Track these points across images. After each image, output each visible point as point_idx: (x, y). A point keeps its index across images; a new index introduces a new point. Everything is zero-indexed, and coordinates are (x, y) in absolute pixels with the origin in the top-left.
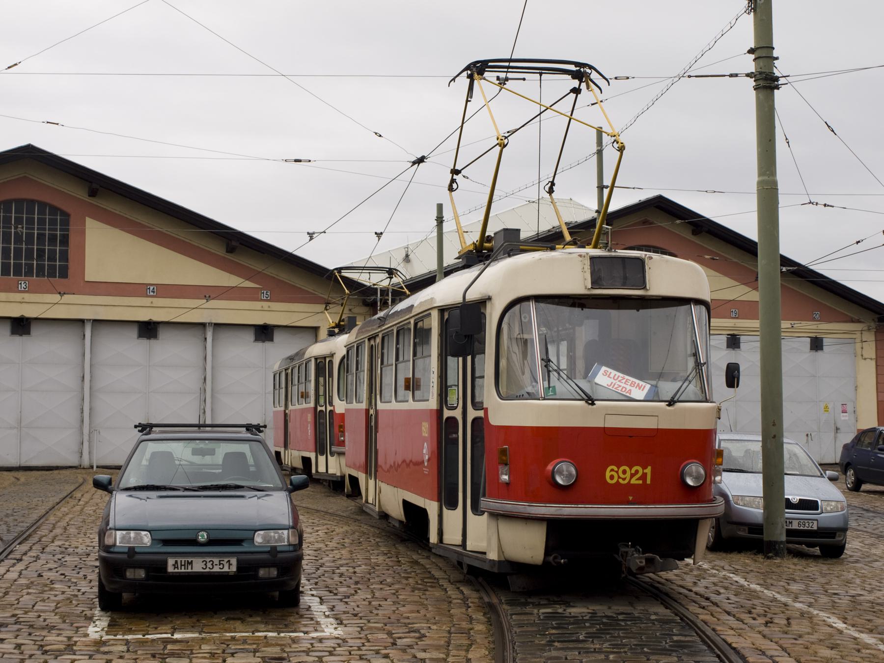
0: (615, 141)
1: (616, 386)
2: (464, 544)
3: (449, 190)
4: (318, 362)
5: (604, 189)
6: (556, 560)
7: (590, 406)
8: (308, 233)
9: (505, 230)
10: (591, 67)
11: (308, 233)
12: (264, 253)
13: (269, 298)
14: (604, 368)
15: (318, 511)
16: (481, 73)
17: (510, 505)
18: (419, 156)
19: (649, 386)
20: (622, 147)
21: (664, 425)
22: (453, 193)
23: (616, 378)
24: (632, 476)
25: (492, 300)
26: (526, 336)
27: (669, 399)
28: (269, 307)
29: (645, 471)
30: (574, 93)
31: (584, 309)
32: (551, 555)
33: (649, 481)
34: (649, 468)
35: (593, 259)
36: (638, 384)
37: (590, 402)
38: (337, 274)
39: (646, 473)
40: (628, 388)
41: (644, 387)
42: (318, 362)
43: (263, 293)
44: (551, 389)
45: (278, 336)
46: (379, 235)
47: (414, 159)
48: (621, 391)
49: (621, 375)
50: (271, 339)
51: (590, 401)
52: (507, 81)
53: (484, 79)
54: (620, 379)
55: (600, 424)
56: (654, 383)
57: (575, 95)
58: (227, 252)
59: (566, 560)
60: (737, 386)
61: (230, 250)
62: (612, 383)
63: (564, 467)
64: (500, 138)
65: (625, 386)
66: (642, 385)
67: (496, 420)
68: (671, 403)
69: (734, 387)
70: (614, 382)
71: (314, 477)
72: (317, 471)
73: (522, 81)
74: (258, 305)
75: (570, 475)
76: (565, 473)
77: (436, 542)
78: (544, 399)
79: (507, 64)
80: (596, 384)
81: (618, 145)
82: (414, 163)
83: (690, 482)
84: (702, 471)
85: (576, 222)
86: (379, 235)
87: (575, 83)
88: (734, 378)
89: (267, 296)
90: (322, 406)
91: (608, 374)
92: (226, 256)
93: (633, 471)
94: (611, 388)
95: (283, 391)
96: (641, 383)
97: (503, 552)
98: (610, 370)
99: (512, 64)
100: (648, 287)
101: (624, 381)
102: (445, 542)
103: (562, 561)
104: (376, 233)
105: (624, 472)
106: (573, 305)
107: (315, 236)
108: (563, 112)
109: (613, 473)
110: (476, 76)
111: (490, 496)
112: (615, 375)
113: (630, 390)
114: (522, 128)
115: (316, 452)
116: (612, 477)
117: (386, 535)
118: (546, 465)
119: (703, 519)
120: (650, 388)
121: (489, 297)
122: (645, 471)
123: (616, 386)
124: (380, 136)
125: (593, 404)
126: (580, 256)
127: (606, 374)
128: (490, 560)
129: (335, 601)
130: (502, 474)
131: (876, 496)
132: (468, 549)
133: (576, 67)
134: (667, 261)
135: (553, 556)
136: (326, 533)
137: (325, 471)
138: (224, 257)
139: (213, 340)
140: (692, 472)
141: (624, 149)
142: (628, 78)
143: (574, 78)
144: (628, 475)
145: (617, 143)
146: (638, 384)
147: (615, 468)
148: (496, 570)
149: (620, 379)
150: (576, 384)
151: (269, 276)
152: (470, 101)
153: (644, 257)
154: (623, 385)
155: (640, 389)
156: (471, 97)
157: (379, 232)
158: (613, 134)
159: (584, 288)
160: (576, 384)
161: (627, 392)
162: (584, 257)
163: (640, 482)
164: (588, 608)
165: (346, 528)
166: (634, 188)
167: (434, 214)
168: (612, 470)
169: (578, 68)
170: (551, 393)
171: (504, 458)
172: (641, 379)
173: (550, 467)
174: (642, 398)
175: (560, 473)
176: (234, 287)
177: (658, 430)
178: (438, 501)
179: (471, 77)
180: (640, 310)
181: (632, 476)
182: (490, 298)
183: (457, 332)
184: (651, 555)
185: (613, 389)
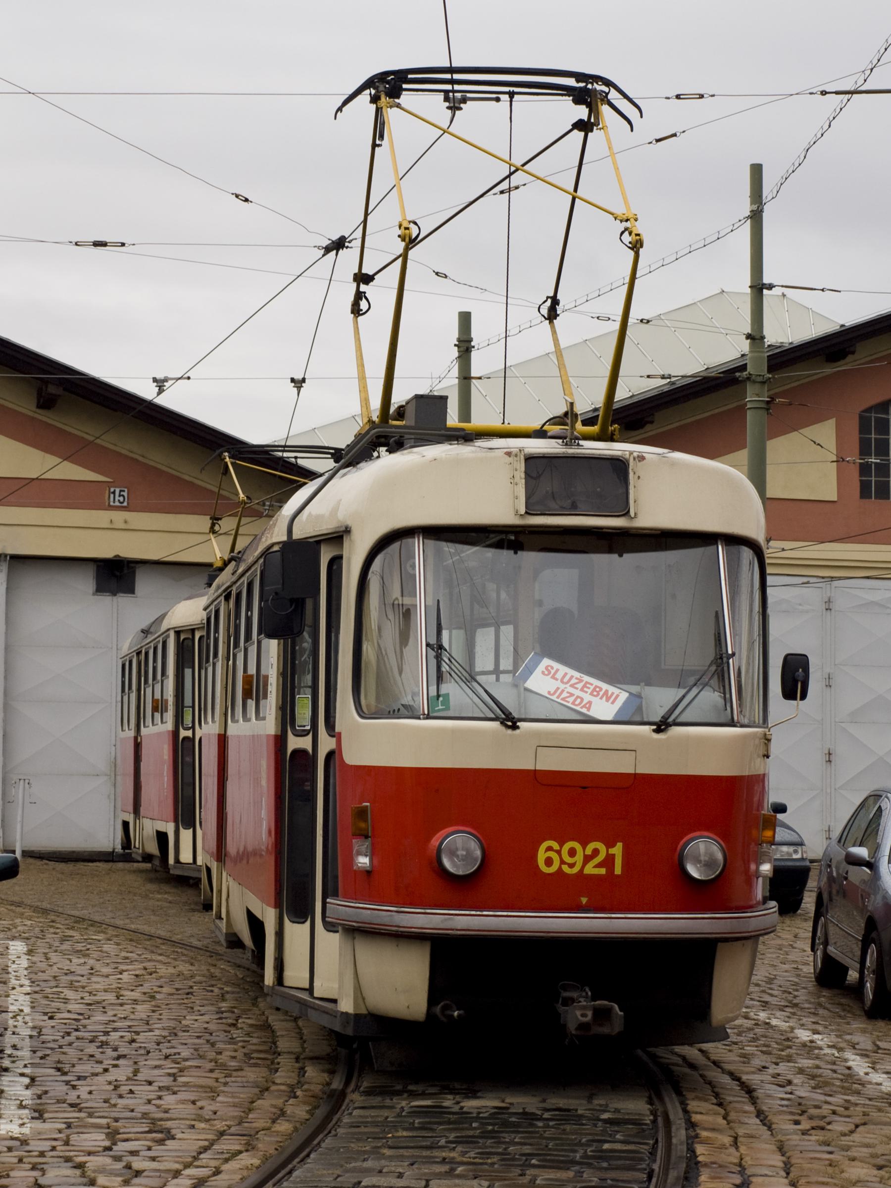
0: (626, 229)
1: (565, 695)
2: (310, 990)
3: (352, 312)
4: (182, 638)
5: (765, 292)
6: (449, 1012)
7: (510, 731)
8: (155, 380)
9: (418, 397)
10: (608, 83)
11: (155, 380)
12: (115, 410)
13: (125, 504)
14: (546, 662)
15: (151, 937)
16: (395, 93)
17: (369, 912)
18: (335, 237)
19: (626, 695)
20: (637, 241)
21: (645, 768)
22: (360, 318)
23: (566, 680)
24: (587, 859)
25: (352, 534)
26: (407, 601)
27: (657, 719)
28: (126, 522)
29: (612, 851)
30: (580, 130)
31: (519, 553)
32: (438, 1004)
33: (618, 870)
34: (620, 845)
35: (531, 460)
36: (607, 691)
37: (510, 723)
38: (227, 460)
39: (614, 855)
40: (587, 697)
41: (618, 696)
42: (182, 638)
43: (114, 493)
44: (441, 699)
45: (144, 583)
46: (298, 383)
47: (326, 243)
48: (573, 703)
49: (577, 674)
50: (131, 590)
51: (510, 721)
52: (465, 103)
53: (398, 106)
54: (574, 681)
55: (526, 764)
56: (635, 689)
57: (583, 134)
58: (39, 406)
59: (461, 1012)
60: (803, 697)
61: (46, 403)
62: (558, 688)
63: (459, 843)
64: (405, 224)
65: (581, 694)
66: (613, 693)
67: (354, 756)
68: (662, 726)
69: (795, 698)
70: (562, 686)
71: (172, 872)
72: (177, 860)
73: (494, 103)
74: (101, 517)
75: (469, 853)
76: (461, 853)
77: (271, 985)
78: (428, 717)
79: (448, 76)
80: (526, 689)
81: (630, 239)
82: (328, 250)
83: (694, 871)
84: (719, 856)
85: (791, 343)
86: (298, 383)
87: (582, 112)
88: (795, 682)
89: (121, 499)
90: (306, 733)
91: (553, 672)
92: (36, 416)
93: (589, 851)
94: (554, 698)
95: (133, 696)
96: (611, 689)
97: (364, 999)
98: (556, 665)
99: (456, 76)
100: (632, 514)
101: (580, 686)
102: (288, 982)
103: (456, 1014)
104: (293, 380)
105: (572, 853)
106: (499, 545)
107: (167, 384)
108: (541, 175)
109: (551, 854)
110: (384, 100)
111: (348, 896)
112: (566, 674)
113: (590, 703)
114: (481, 199)
115: (176, 821)
116: (549, 862)
117: (253, 982)
118: (429, 839)
119: (726, 940)
120: (628, 698)
121: (346, 528)
122: (612, 851)
123: (565, 695)
124: (246, 200)
125: (514, 727)
126: (509, 454)
127: (550, 672)
128: (342, 1013)
129: (57, 1083)
130: (359, 853)
131: (264, 835)
132: (316, 995)
133: (578, 81)
134: (674, 464)
135: (442, 1004)
136: (137, 976)
137: (191, 861)
138: (33, 418)
139: (7, 589)
140: (700, 855)
141: (642, 246)
142: (701, 96)
143: (577, 101)
144: (579, 858)
145: (630, 234)
146: (607, 691)
147: (556, 846)
148: (349, 1031)
149: (574, 681)
150: (486, 691)
151: (126, 457)
152: (379, 145)
153: (627, 456)
154: (577, 693)
155: (608, 700)
156: (382, 137)
157: (298, 376)
158: (625, 217)
159: (512, 513)
160: (486, 691)
161: (584, 706)
162: (516, 455)
163: (603, 871)
164: (503, 1101)
165: (184, 968)
166: (823, 290)
167: (454, 334)
168: (549, 849)
169: (582, 85)
170: (440, 707)
171: (362, 825)
172: (611, 681)
173: (435, 842)
174: (610, 718)
175: (452, 853)
176: (33, 479)
177: (635, 776)
178: (275, 907)
179: (375, 99)
180: (625, 555)
181: (587, 859)
182: (347, 531)
183: (276, 593)
184: (606, 1002)
185: (559, 700)
